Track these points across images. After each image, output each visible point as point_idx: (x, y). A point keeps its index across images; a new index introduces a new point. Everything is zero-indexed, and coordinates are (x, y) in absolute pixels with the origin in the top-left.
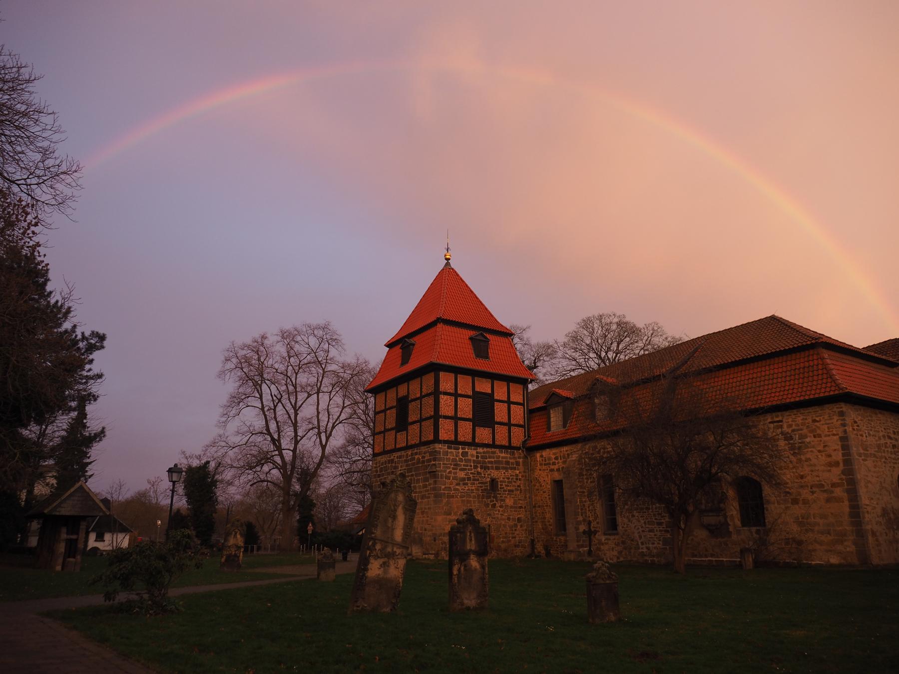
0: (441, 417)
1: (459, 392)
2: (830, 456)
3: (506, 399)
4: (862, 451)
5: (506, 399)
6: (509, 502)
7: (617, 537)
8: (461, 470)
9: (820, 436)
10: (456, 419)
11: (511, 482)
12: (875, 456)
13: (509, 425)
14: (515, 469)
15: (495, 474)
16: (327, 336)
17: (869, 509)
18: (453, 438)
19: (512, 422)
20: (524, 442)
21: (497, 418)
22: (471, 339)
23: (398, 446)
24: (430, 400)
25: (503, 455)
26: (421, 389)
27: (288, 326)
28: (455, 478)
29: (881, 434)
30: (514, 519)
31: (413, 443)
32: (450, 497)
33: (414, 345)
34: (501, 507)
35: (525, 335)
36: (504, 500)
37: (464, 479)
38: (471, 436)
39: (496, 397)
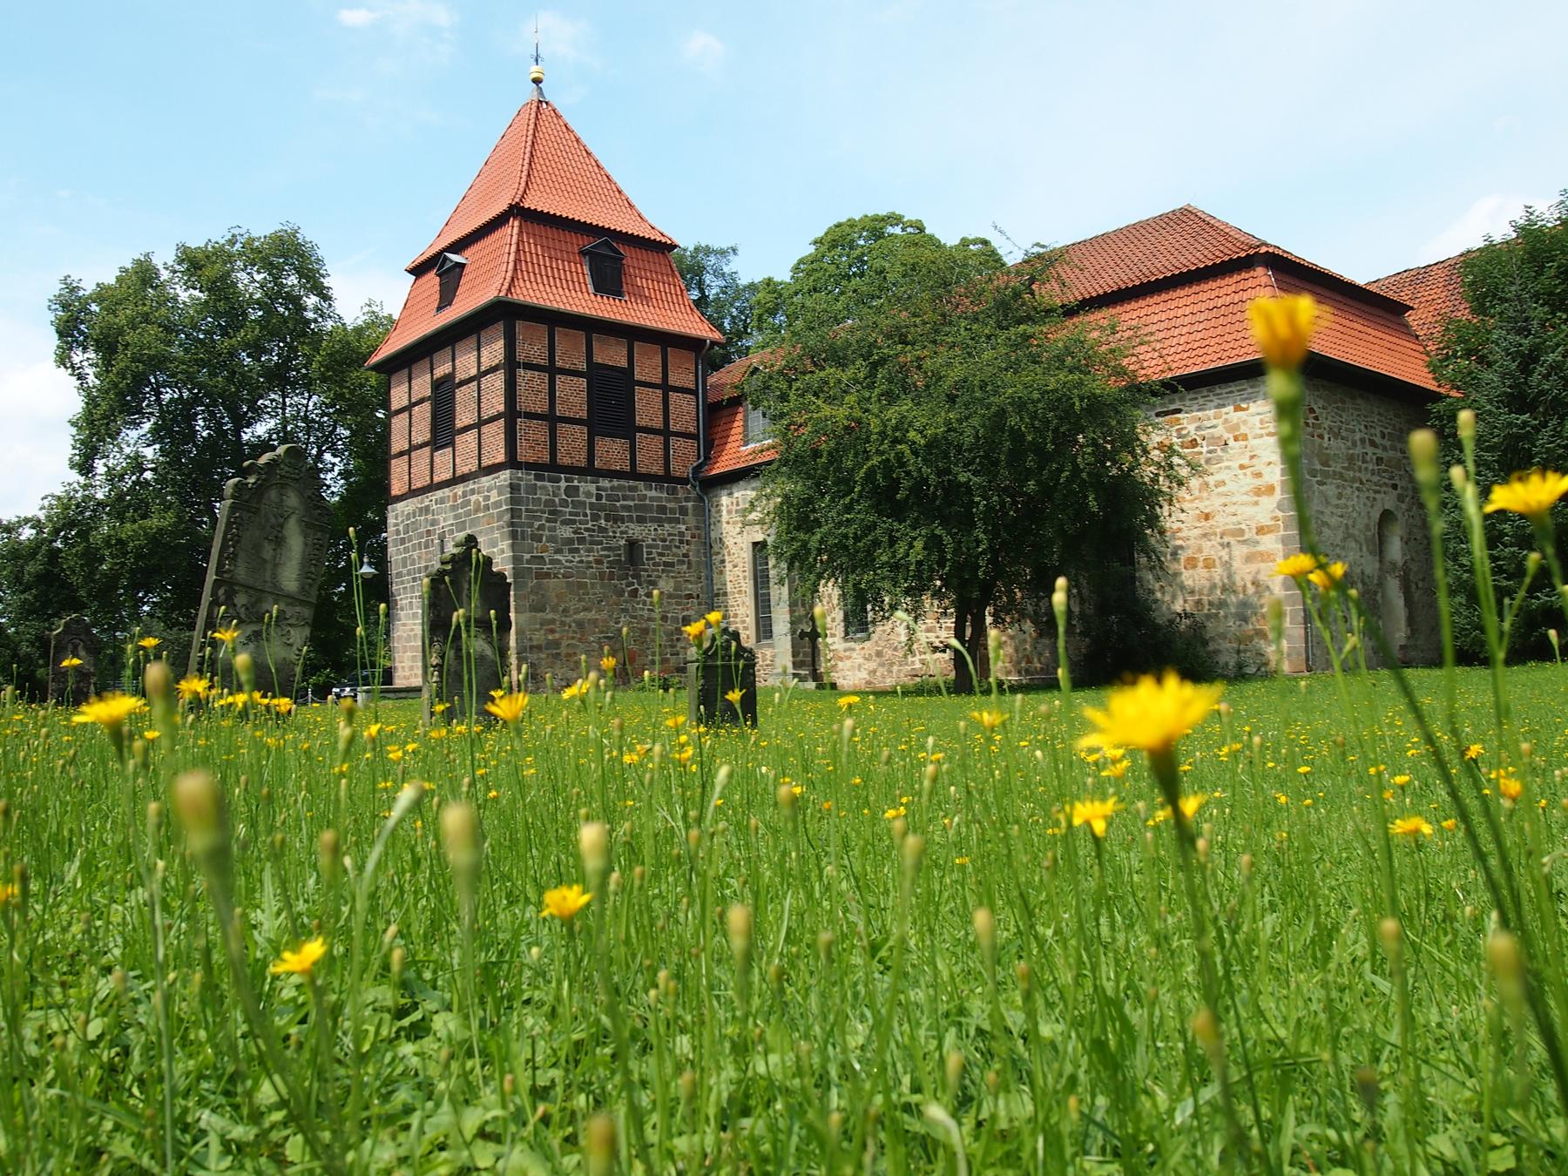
1: (559, 364)
3: (659, 381)
4: (1318, 467)
8: (564, 523)
9: (1245, 437)
10: (552, 419)
12: (1342, 476)
13: (665, 433)
14: (677, 521)
15: (635, 530)
16: (289, 256)
18: (546, 458)
20: (697, 470)
21: (641, 420)
23: (436, 479)
25: (653, 493)
27: (196, 242)
28: (552, 539)
29: (1358, 436)
30: (675, 619)
31: (466, 470)
32: (541, 575)
33: (463, 265)
37: (570, 541)
38: (584, 454)
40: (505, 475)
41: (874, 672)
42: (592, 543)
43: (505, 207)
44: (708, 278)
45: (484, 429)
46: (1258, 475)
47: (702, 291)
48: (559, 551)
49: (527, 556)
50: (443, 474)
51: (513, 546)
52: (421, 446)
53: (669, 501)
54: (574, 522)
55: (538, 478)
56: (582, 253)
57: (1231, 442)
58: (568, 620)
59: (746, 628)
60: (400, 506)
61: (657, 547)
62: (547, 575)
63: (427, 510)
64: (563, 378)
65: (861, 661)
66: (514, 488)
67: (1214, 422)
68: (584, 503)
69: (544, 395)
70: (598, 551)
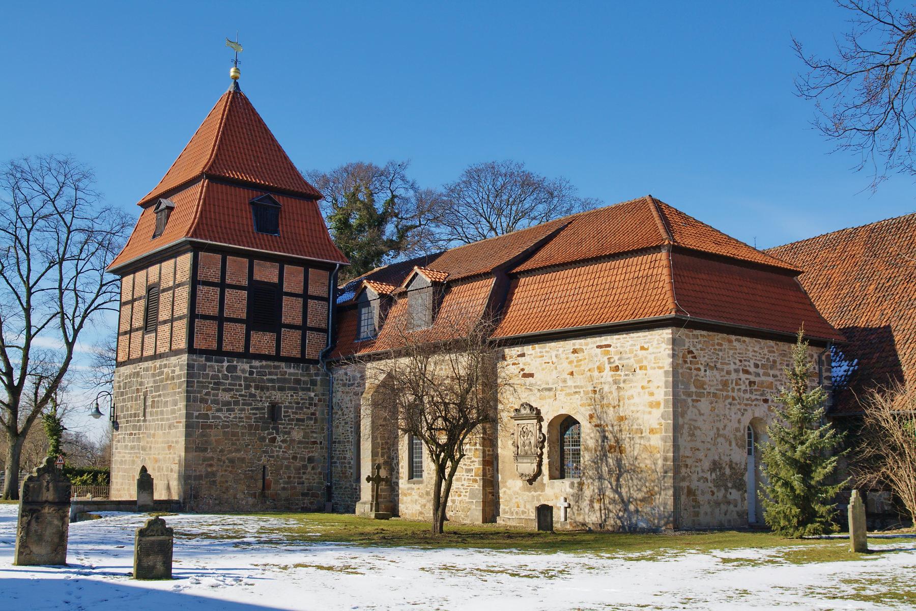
1: (228, 281)
2: (652, 394)
3: (301, 292)
5: (301, 292)
7: (421, 486)
8: (224, 390)
10: (221, 319)
11: (301, 408)
14: (309, 390)
15: (277, 396)
17: (689, 462)
18: (215, 346)
19: (309, 324)
22: (252, 203)
23: (145, 354)
25: (292, 370)
28: (215, 402)
30: (303, 459)
34: (283, 441)
35: (409, 175)
36: (289, 433)
38: (243, 343)
41: (425, 506)
46: (652, 394)
50: (149, 352)
52: (137, 330)
53: (302, 375)
54: (233, 390)
55: (207, 360)
57: (638, 371)
59: (350, 468)
62: (210, 427)
63: (137, 374)
64: (230, 291)
65: (417, 497)
66: (190, 366)
67: (629, 356)
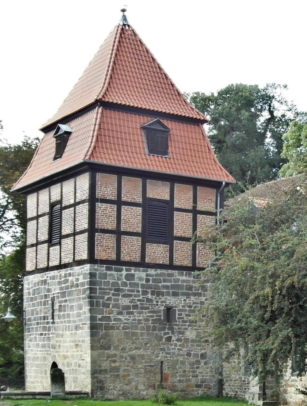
0: (97, 230)
1: (124, 199)
3: (190, 208)
6: (190, 334)
8: (124, 296)
10: (118, 233)
14: (200, 295)
15: (171, 301)
18: (114, 257)
21: (177, 232)
24: (84, 210)
25: (184, 278)
26: (75, 193)
28: (115, 306)
30: (196, 355)
32: (107, 328)
34: (178, 340)
36: (183, 333)
37: (128, 307)
38: (139, 254)
39: (176, 205)
40: (87, 267)
42: (142, 308)
43: (93, 101)
44: (275, 104)
45: (77, 237)
47: (271, 113)
48: (120, 313)
49: (99, 316)
50: (54, 262)
51: (91, 310)
52: (43, 242)
56: (143, 128)
58: (125, 355)
60: (31, 278)
61: (185, 311)
62: (112, 328)
63: (45, 282)
66: (92, 275)
68: (138, 284)
69: (114, 218)
70: (146, 314)
